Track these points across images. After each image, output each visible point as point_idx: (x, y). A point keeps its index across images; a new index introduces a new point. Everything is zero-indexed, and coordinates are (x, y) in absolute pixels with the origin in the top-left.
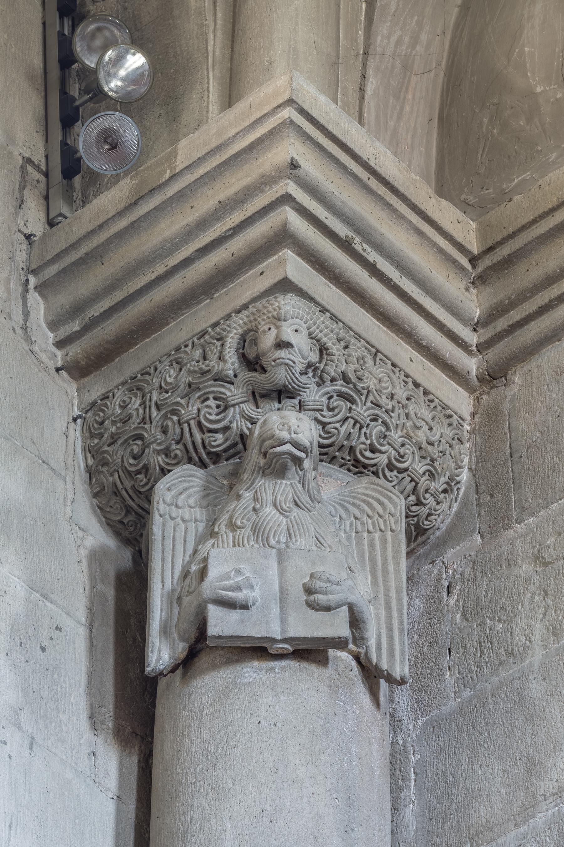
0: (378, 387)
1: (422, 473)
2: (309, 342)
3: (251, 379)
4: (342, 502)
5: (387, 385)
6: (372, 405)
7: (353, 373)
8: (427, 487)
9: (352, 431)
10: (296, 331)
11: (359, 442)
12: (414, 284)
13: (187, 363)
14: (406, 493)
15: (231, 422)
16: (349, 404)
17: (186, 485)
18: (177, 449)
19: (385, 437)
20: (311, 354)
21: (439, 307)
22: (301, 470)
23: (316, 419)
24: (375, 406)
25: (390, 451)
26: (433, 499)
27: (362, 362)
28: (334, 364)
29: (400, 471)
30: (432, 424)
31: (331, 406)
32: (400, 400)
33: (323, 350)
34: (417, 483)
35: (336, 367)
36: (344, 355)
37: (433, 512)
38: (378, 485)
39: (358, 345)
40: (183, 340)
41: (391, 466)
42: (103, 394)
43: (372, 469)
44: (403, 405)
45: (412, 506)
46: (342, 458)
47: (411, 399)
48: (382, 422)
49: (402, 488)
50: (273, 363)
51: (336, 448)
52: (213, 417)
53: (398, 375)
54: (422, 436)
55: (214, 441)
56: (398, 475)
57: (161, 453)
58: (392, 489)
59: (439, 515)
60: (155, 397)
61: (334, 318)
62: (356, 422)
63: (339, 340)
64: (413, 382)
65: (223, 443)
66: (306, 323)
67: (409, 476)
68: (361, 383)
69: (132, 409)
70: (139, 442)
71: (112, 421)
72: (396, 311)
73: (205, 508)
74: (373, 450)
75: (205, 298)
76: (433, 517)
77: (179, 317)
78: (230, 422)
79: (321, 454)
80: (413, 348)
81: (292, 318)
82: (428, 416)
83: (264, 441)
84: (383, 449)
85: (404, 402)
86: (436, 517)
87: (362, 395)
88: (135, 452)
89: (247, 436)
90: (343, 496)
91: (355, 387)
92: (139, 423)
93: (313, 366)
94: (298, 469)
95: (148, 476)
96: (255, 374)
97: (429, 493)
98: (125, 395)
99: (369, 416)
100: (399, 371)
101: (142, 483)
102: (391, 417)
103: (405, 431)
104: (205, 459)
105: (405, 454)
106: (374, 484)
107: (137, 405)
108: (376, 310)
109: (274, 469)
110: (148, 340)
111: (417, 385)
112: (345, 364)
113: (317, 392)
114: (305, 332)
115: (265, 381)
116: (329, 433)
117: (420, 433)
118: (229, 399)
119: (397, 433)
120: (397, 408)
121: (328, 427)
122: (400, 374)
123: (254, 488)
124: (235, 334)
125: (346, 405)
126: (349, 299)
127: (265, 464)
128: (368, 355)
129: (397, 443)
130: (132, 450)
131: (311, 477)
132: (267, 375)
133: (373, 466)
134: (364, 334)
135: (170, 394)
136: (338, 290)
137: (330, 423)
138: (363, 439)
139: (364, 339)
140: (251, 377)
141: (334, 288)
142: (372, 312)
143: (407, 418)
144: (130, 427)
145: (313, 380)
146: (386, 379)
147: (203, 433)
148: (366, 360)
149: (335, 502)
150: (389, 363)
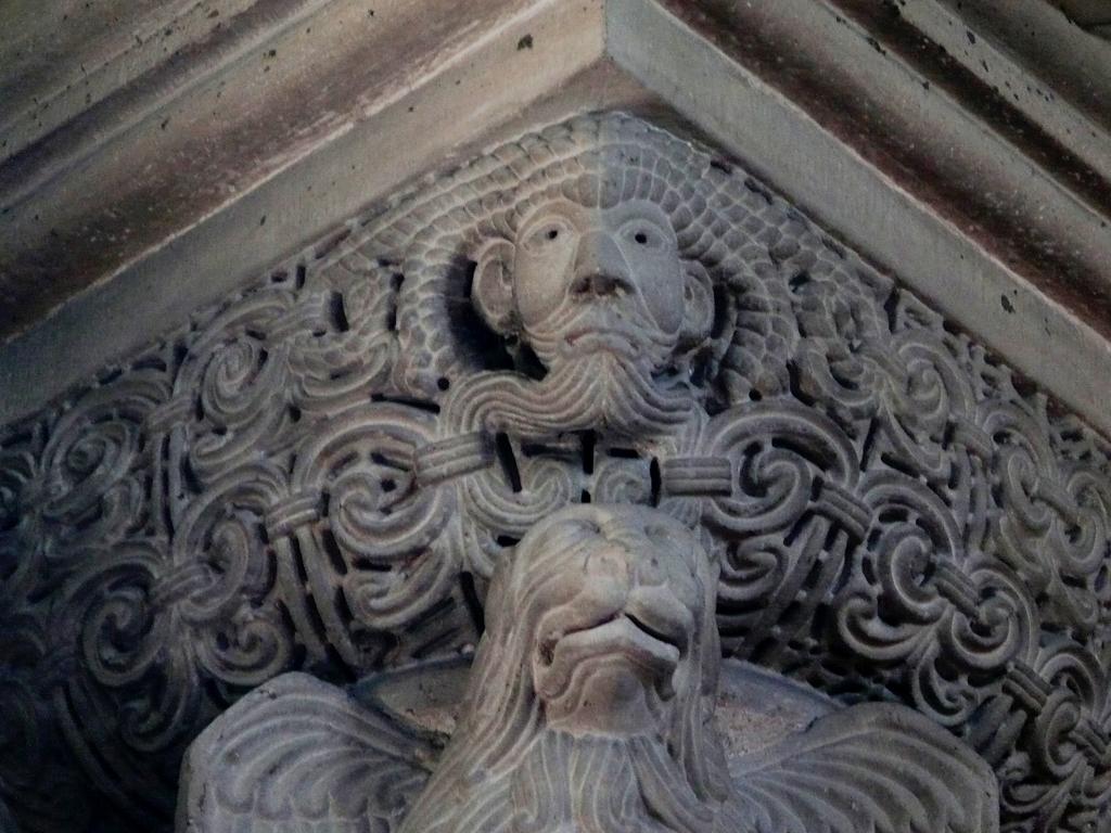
0: (904, 405)
1: (1047, 679)
2: (683, 271)
3: (493, 393)
4: (795, 790)
5: (931, 395)
6: (885, 467)
7: (825, 366)
8: (1066, 724)
9: (823, 555)
10: (641, 238)
11: (846, 591)
12: (1013, 58)
13: (284, 334)
14: (995, 749)
15: (434, 534)
16: (812, 470)
17: (286, 741)
18: (256, 622)
19: (930, 570)
20: (689, 307)
21: (1092, 128)
22: (665, 699)
23: (709, 523)
24: (893, 471)
25: (946, 614)
26: (1084, 761)
27: (850, 325)
28: (762, 340)
29: (980, 677)
30: (1079, 514)
31: (755, 476)
32: (976, 443)
33: (728, 295)
34: (1033, 713)
35: (771, 346)
36: (793, 304)
37: (1085, 801)
38: (911, 730)
39: (839, 268)
40: (267, 255)
41: (949, 664)
42: (12, 426)
43: (887, 674)
44: (983, 460)
45: (1017, 784)
46: (795, 645)
47: (1008, 435)
48: (919, 522)
49: (985, 733)
50: (568, 348)
51: (774, 612)
52: (370, 518)
53: (965, 358)
54: (1047, 554)
55: (380, 594)
56: (971, 690)
57: (204, 633)
58: (952, 740)
59: (1103, 809)
60: (180, 447)
61: (761, 186)
62: (837, 526)
63: (776, 257)
64: (1013, 378)
65: (407, 602)
66: (670, 208)
67: (1007, 690)
68: (849, 398)
69: (109, 482)
70: (133, 594)
71: (45, 519)
72: (957, 151)
73: (355, 816)
74: (892, 612)
75: (339, 119)
76: (1084, 816)
77: (254, 179)
78: (428, 533)
79: (725, 632)
80: (1010, 262)
81: (627, 196)
82: (1064, 488)
83: (541, 607)
84: (924, 608)
85: (989, 447)
86: (1094, 815)
87: (854, 438)
88: (122, 624)
89: (487, 580)
90: (800, 769)
91: (832, 411)
92: (132, 531)
93: (695, 346)
94: (656, 697)
95: (165, 705)
96: (504, 379)
97: (1072, 741)
98: (84, 432)
99: (877, 504)
100: (970, 345)
101: (143, 728)
102: (948, 503)
103: (992, 545)
104: (345, 656)
105: (996, 621)
106: (897, 727)
107: (120, 473)
108: (893, 149)
109: (576, 697)
110: (156, 248)
111: (1026, 387)
112: (796, 335)
113: (711, 434)
114: (669, 239)
115: (542, 403)
116: (750, 564)
117: (1039, 547)
118: (425, 459)
119: (966, 554)
120: (966, 471)
121: (746, 544)
122: (972, 355)
123: (513, 760)
124: (443, 240)
125: (804, 474)
126: (805, 116)
127: (547, 682)
128: (871, 301)
129: (967, 588)
130: (111, 619)
131: (697, 716)
132: (549, 381)
133: (898, 662)
134: (857, 232)
135: (229, 436)
136: (769, 90)
137: (751, 534)
138: (859, 580)
139: (856, 248)
140: (494, 387)
141: (756, 82)
142: (879, 154)
143: (999, 503)
144: (103, 540)
145: (696, 392)
146: (928, 375)
147: (341, 568)
148: (863, 316)
149: (771, 788)
150: (937, 320)
